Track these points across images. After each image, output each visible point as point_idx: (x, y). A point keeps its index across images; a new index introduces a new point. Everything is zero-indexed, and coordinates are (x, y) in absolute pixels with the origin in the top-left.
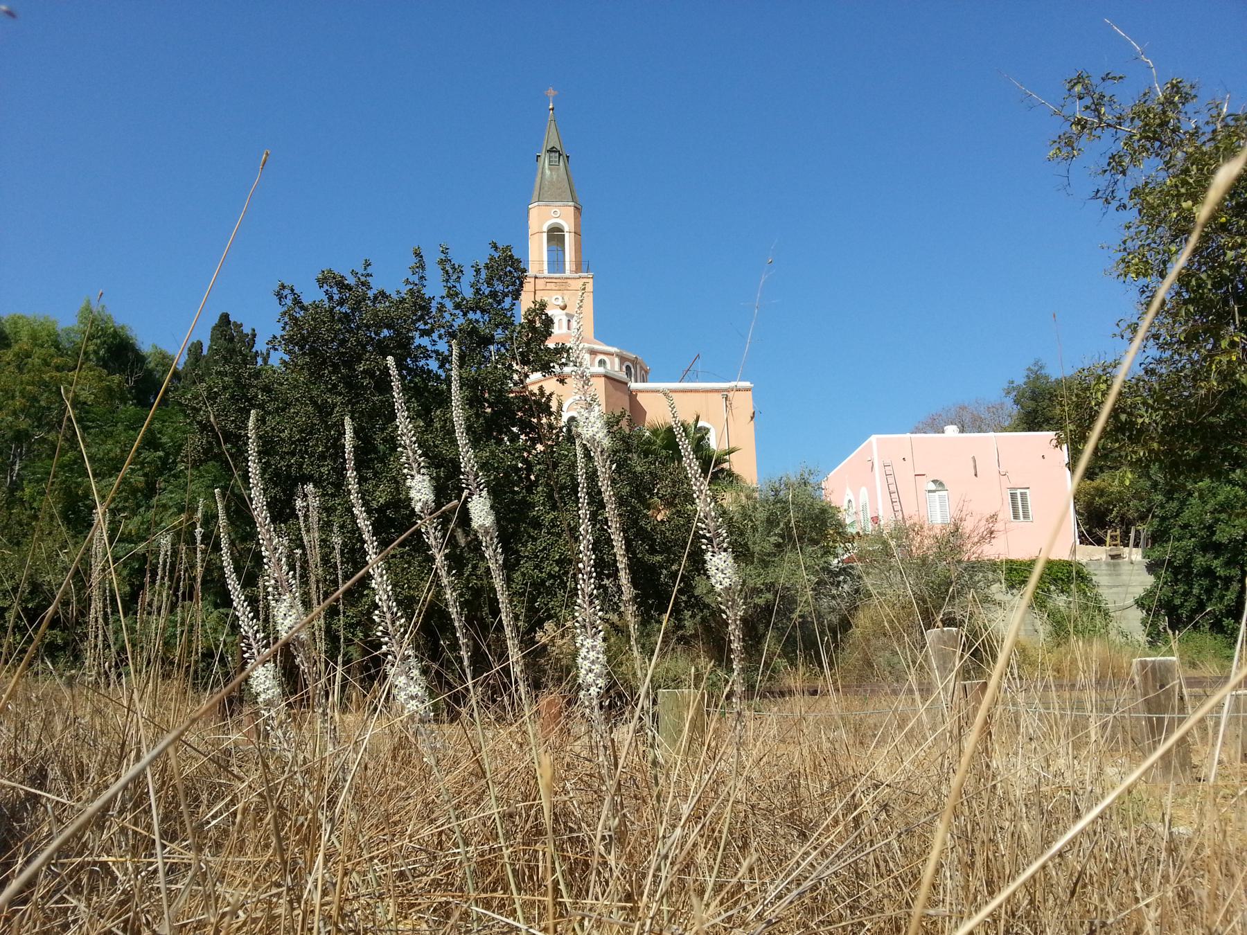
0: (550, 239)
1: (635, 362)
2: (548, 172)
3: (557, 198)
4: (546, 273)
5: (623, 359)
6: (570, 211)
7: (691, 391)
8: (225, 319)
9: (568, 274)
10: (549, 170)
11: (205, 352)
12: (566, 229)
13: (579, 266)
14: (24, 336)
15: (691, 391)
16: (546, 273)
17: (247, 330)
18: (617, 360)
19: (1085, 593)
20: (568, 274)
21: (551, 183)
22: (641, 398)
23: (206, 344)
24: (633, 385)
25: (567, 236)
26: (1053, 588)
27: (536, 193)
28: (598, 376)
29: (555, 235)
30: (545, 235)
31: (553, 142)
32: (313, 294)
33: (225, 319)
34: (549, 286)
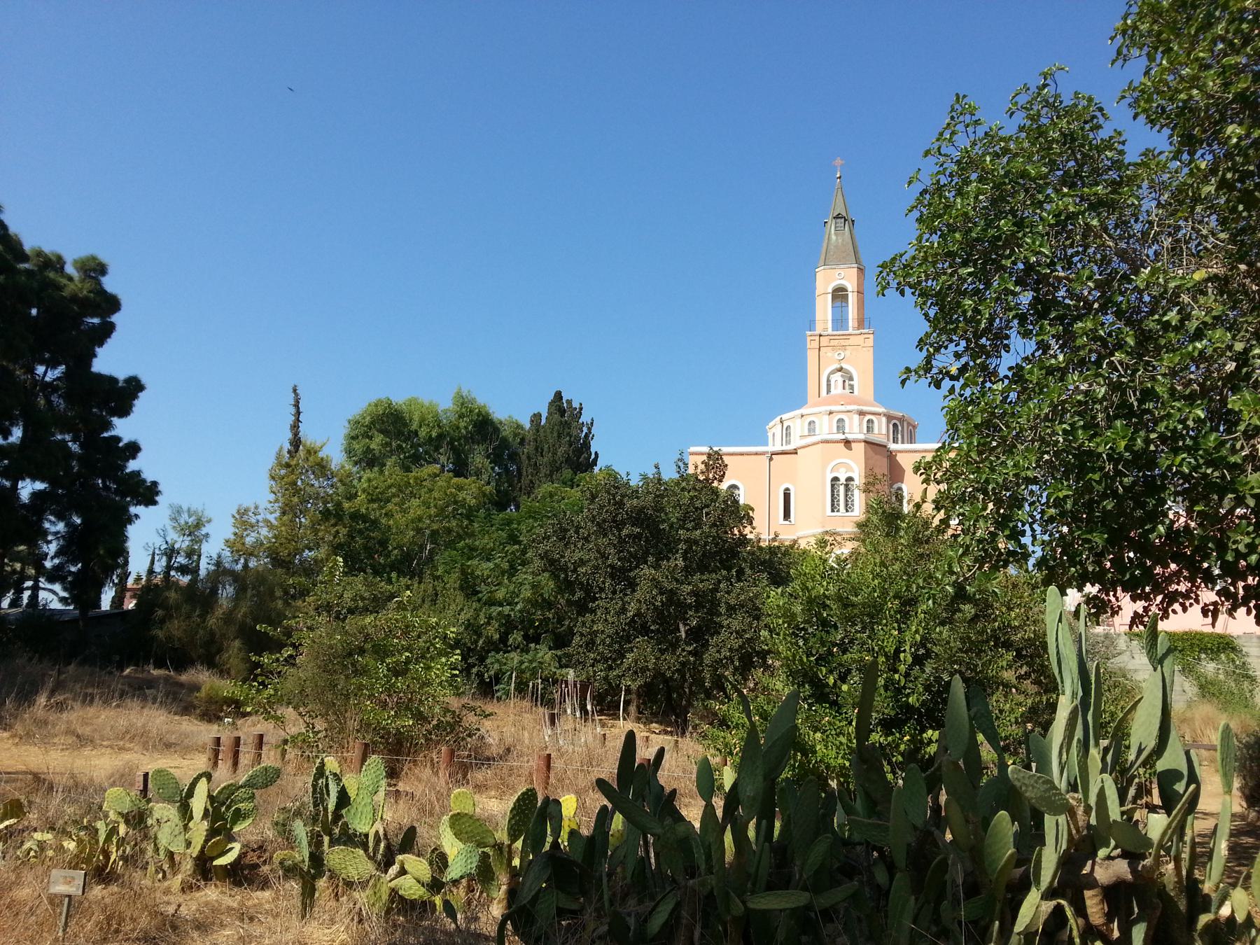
0: (834, 298)
1: (902, 420)
2: (834, 237)
3: (841, 262)
4: (830, 331)
5: (889, 418)
6: (853, 272)
7: (742, 454)
8: (558, 396)
9: (850, 331)
10: (835, 236)
11: (543, 421)
12: (850, 289)
13: (861, 323)
14: (416, 418)
15: (742, 454)
16: (830, 331)
17: (576, 405)
18: (884, 420)
19: (1233, 661)
20: (850, 331)
21: (836, 247)
22: (900, 458)
23: (544, 415)
24: (892, 446)
25: (850, 295)
26: (1203, 656)
27: (823, 257)
28: (859, 441)
29: (839, 294)
30: (830, 296)
31: (840, 209)
32: (585, 418)
33: (558, 396)
34: (833, 343)
